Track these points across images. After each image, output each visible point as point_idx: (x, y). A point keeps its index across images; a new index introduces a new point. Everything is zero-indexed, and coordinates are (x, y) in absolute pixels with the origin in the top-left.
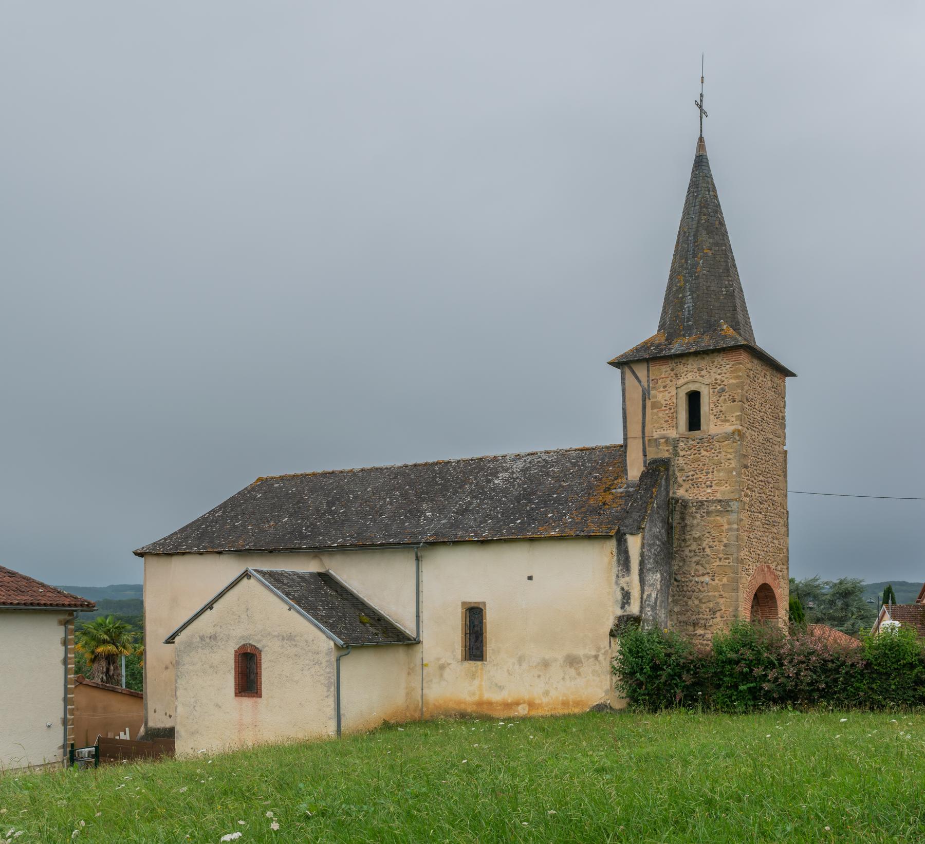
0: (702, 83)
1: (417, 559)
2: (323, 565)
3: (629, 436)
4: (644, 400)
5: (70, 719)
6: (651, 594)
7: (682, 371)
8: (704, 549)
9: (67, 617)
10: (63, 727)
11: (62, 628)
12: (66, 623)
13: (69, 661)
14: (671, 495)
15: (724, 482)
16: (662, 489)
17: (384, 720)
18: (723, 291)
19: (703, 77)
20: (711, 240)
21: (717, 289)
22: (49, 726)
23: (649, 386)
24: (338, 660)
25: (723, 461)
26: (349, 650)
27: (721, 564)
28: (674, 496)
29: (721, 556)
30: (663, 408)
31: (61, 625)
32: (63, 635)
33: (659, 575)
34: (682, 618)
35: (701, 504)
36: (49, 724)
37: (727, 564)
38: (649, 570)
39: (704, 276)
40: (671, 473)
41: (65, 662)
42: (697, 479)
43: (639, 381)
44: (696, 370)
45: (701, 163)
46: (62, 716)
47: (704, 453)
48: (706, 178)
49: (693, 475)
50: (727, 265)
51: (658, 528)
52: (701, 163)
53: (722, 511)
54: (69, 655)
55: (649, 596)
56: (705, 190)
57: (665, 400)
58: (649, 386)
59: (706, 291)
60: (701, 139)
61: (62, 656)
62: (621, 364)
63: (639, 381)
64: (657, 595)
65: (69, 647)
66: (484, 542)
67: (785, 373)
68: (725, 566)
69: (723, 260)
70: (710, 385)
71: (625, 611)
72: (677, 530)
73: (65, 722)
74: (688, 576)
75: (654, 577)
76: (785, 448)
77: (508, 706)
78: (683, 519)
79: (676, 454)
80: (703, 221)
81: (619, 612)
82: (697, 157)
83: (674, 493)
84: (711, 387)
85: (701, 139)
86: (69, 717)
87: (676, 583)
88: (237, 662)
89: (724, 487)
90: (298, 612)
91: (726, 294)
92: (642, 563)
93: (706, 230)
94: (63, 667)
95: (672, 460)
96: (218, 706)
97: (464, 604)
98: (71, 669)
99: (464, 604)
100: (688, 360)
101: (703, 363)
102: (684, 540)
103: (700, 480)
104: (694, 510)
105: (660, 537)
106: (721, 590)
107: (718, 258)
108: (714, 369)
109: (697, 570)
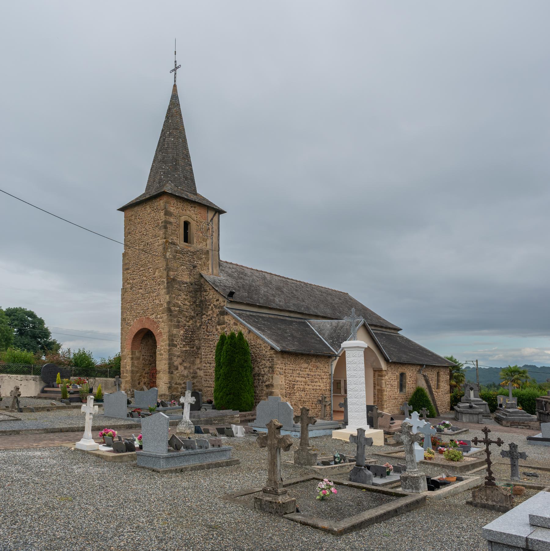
60: (175, 86)
85: (175, 86)
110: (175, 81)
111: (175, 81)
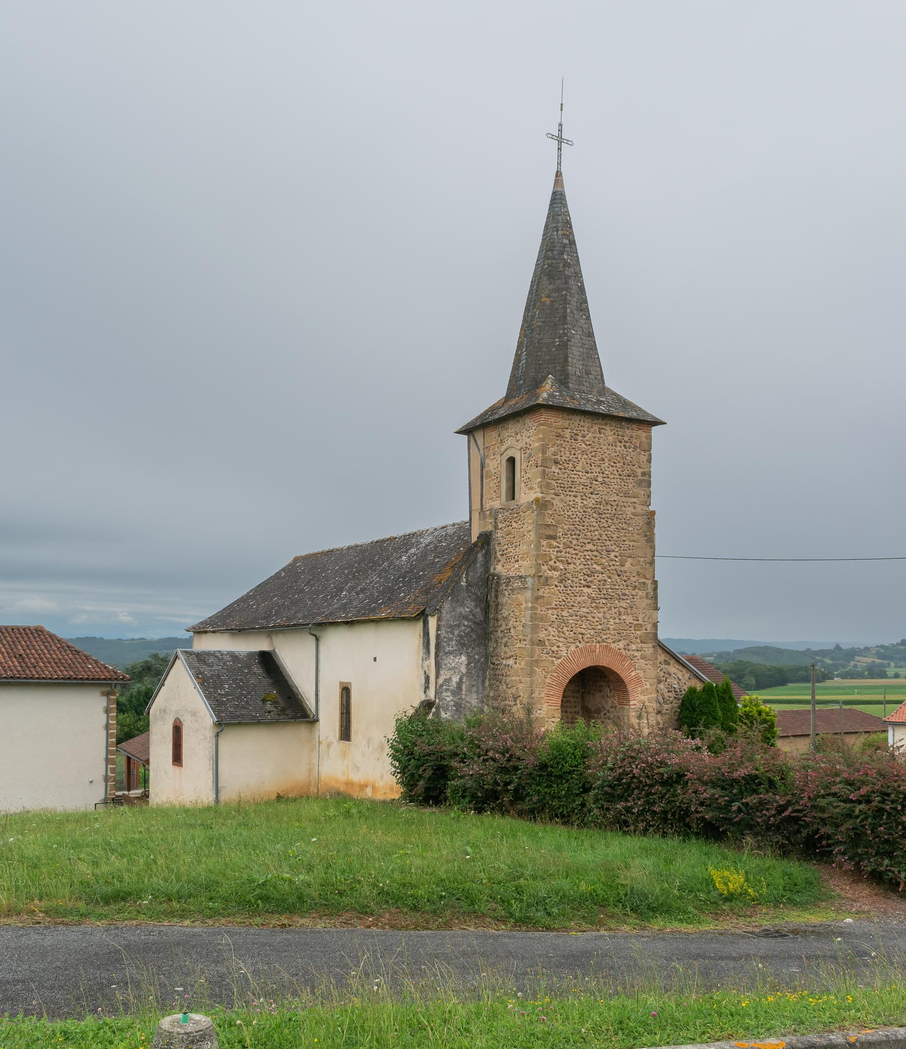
0: (562, 110)
1: (317, 639)
2: (272, 644)
3: (473, 509)
4: (482, 470)
5: (112, 777)
6: (450, 679)
7: (505, 436)
8: (510, 629)
9: (108, 689)
10: (104, 783)
11: (105, 698)
12: (108, 694)
13: (111, 727)
14: (492, 571)
15: (525, 556)
16: (478, 565)
17: (278, 793)
18: (555, 342)
19: (562, 104)
20: (551, 287)
21: (549, 341)
22: (91, 782)
23: (484, 453)
24: (217, 735)
25: (526, 533)
26: (222, 727)
27: (521, 646)
28: (494, 571)
29: (520, 637)
30: (493, 478)
31: (104, 696)
32: (105, 705)
33: (464, 658)
34: (496, 704)
35: (509, 579)
36: (90, 780)
37: (524, 646)
38: (450, 653)
39: (538, 329)
40: (491, 547)
41: (107, 727)
42: (509, 553)
43: (479, 450)
44: (513, 435)
45: (558, 199)
46: (104, 773)
47: (514, 525)
48: (556, 217)
49: (506, 549)
50: (565, 312)
51: (468, 607)
52: (558, 199)
53: (521, 588)
54: (111, 722)
55: (448, 681)
56: (553, 231)
57: (495, 469)
58: (484, 453)
59: (537, 344)
60: (558, 174)
61: (104, 722)
62: (469, 431)
63: (479, 450)
64: (461, 679)
65: (111, 715)
66: (349, 623)
67: (648, 423)
68: (523, 648)
69: (561, 306)
70: (522, 450)
71: (426, 696)
72: (492, 610)
73: (106, 779)
74: (500, 658)
75: (457, 660)
76: (651, 508)
77: (363, 787)
78: (497, 597)
79: (496, 527)
80: (546, 266)
81: (423, 697)
82: (553, 193)
83: (495, 569)
84: (523, 452)
85: (558, 174)
86: (109, 774)
87: (492, 666)
88: (173, 730)
89: (526, 562)
90: (198, 690)
91: (558, 345)
92: (438, 645)
93: (548, 275)
94: (105, 731)
95: (493, 533)
96: (166, 773)
97: (341, 683)
98: (112, 733)
99: (341, 683)
100: (508, 424)
101: (518, 426)
102: (497, 620)
103: (511, 554)
104: (504, 588)
105: (471, 617)
106: (520, 674)
107: (556, 305)
108: (526, 432)
109: (505, 653)
110: (559, 164)
111: (559, 164)
